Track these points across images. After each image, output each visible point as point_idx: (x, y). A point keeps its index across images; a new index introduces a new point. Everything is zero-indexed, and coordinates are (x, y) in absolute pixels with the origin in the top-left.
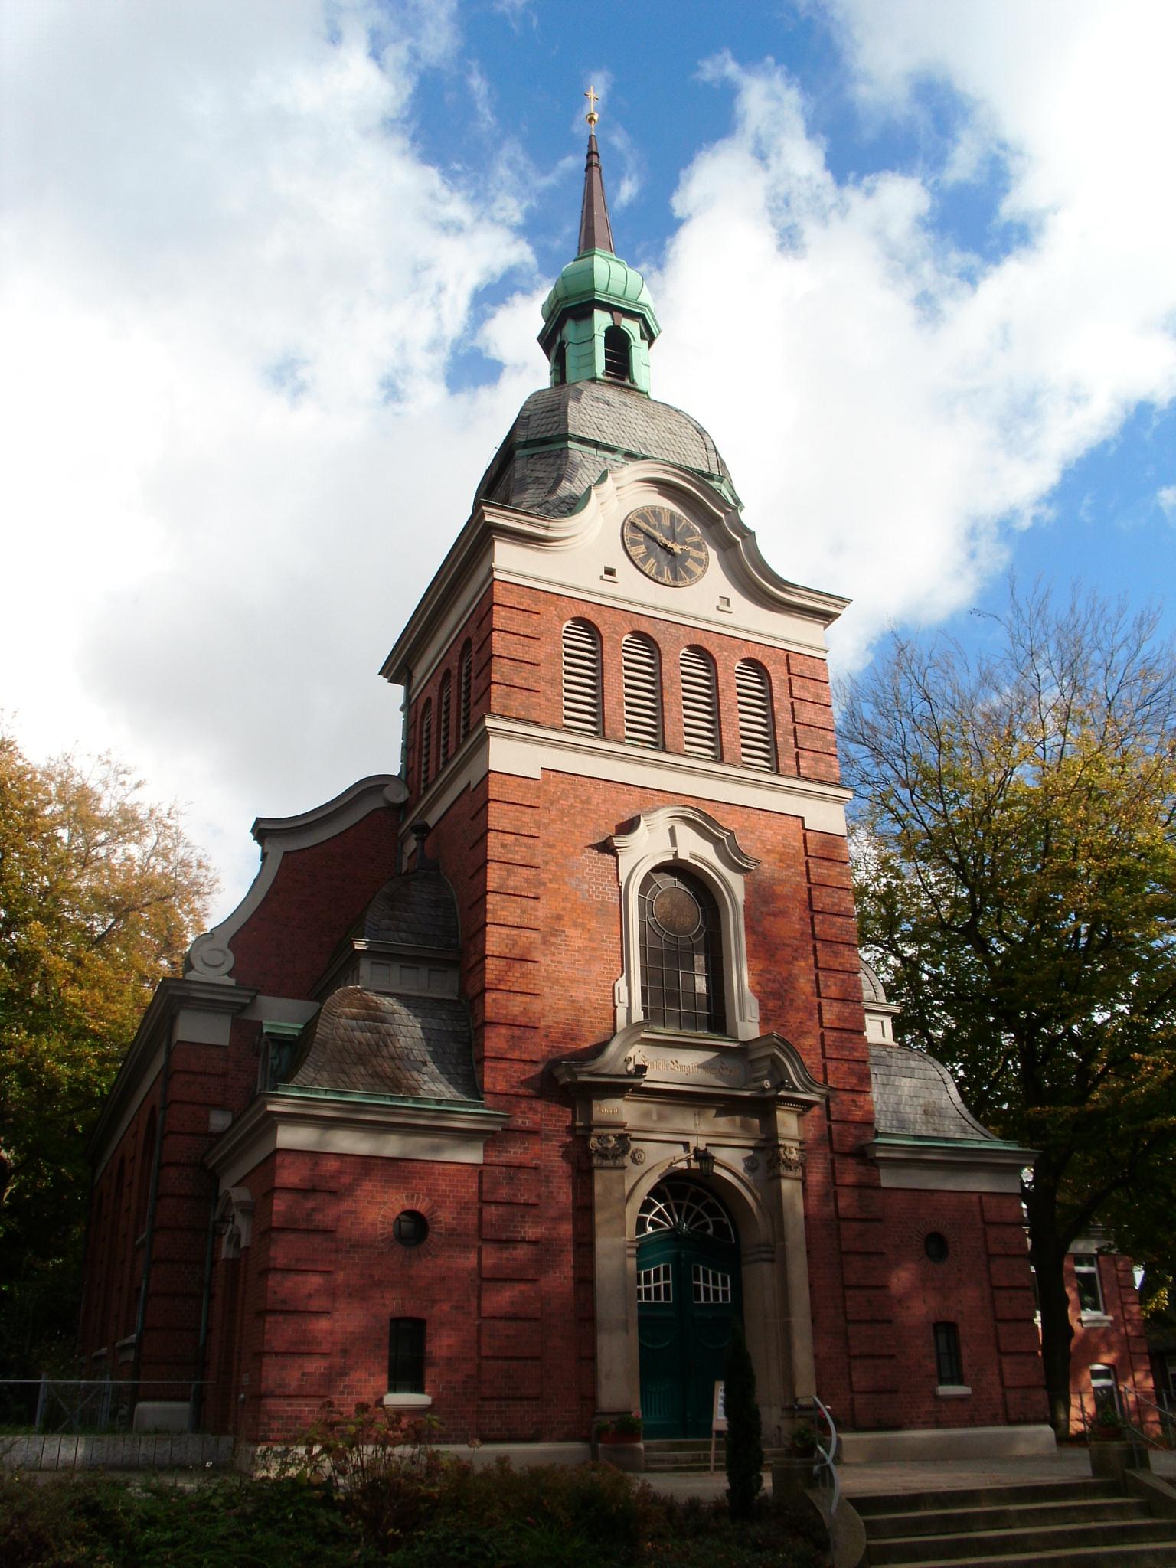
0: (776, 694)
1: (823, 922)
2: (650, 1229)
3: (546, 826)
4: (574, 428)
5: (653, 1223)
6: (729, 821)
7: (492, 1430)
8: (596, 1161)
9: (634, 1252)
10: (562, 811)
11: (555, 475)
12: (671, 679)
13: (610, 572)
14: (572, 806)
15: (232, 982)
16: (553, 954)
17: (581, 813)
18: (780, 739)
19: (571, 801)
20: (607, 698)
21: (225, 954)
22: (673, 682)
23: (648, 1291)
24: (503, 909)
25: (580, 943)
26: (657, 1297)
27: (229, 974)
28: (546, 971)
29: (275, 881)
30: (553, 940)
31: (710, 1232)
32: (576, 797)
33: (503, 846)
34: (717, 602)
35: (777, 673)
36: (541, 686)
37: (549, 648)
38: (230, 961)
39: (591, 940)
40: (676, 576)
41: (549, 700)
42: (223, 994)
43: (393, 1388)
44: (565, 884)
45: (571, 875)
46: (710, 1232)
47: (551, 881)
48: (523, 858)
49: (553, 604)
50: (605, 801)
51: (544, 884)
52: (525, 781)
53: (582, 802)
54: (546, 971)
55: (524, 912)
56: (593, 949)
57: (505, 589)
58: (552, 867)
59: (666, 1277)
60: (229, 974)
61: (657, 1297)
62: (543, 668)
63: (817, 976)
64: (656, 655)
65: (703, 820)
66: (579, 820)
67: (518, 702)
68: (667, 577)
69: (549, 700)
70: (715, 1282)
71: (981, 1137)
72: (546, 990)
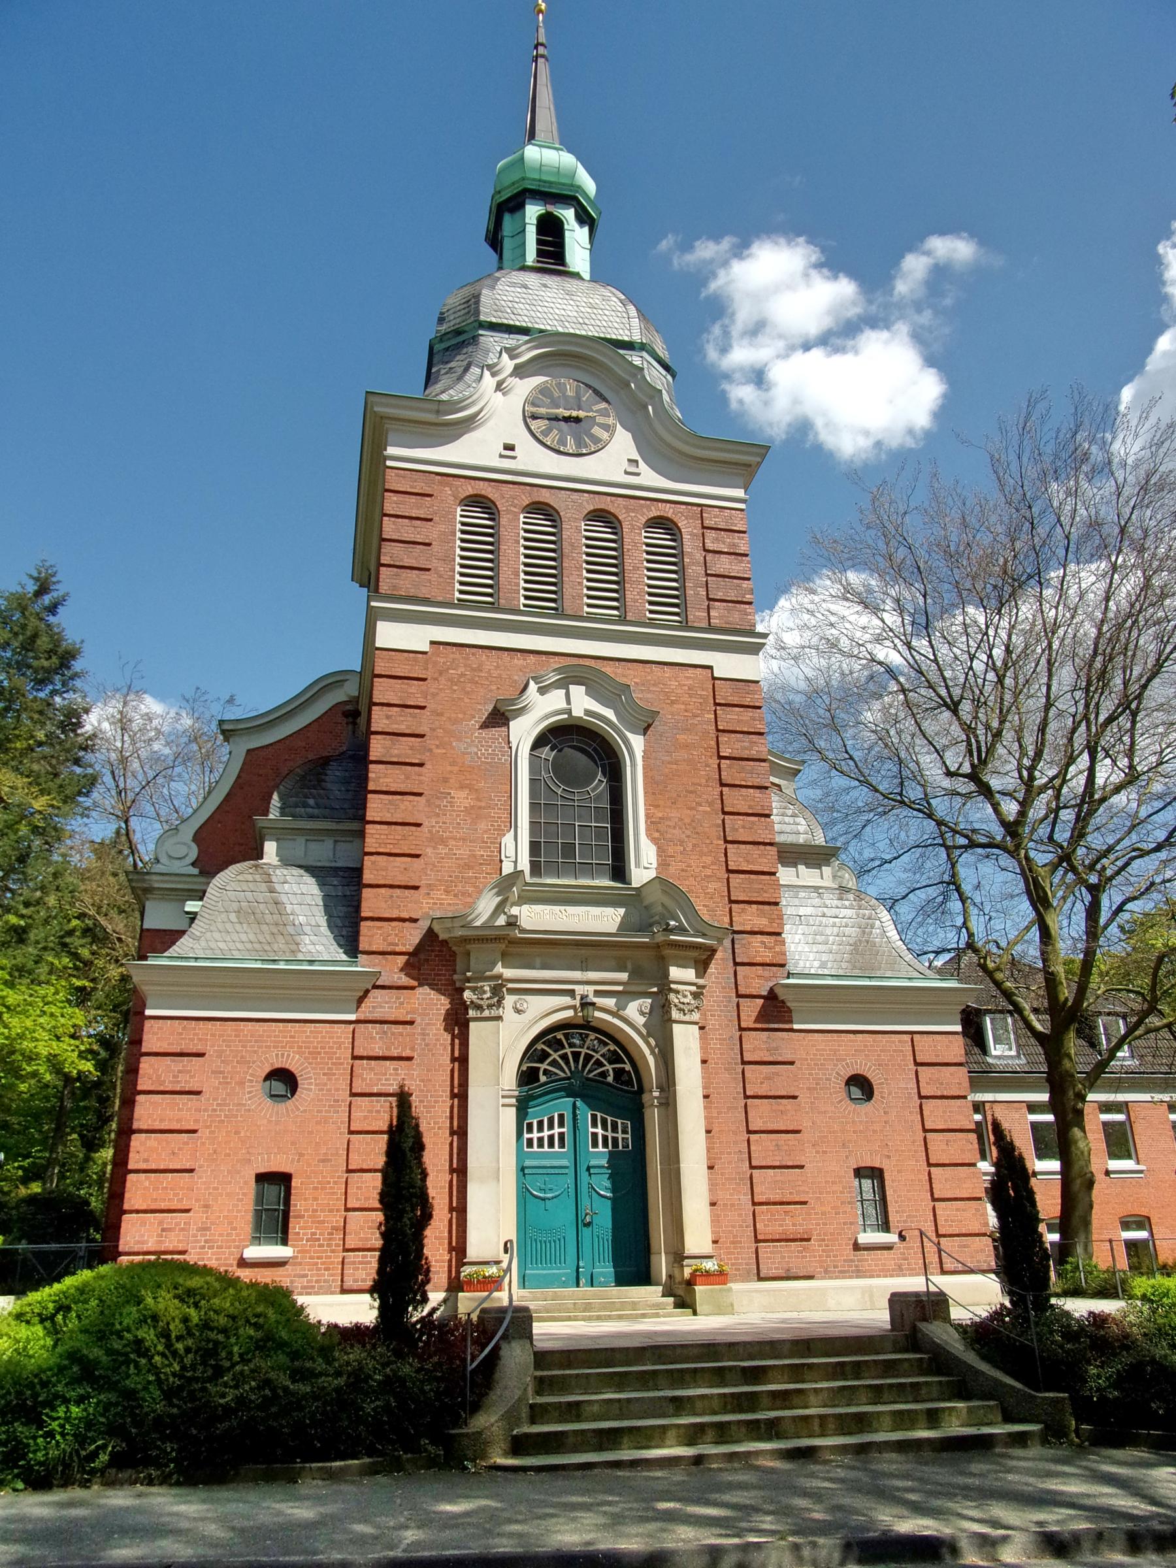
0: (687, 549)
1: (730, 767)
2: (543, 1079)
3: (434, 695)
4: (487, 314)
5: (546, 1072)
6: (629, 676)
7: (356, 1281)
8: (472, 1013)
9: (514, 1101)
10: (450, 680)
11: (465, 363)
12: (572, 545)
13: (510, 447)
14: (462, 675)
15: (196, 871)
16: (438, 815)
17: (472, 681)
18: (690, 592)
19: (461, 670)
20: (503, 568)
21: (189, 847)
22: (636, 568)
23: (540, 1140)
24: (386, 776)
25: (466, 803)
26: (551, 1145)
27: (193, 864)
28: (430, 832)
29: (239, 777)
30: (438, 802)
31: (610, 1079)
32: (465, 666)
33: (388, 717)
34: (626, 465)
35: (688, 528)
36: (434, 564)
37: (442, 527)
38: (194, 852)
39: (478, 799)
40: (579, 443)
41: (441, 576)
42: (185, 882)
43: (257, 1240)
44: (453, 748)
45: (459, 740)
46: (610, 1079)
47: (438, 747)
48: (408, 727)
49: (448, 485)
50: (497, 667)
51: (430, 750)
52: (411, 655)
53: (473, 670)
54: (430, 832)
55: (407, 778)
56: (480, 808)
57: (397, 475)
58: (440, 732)
59: (561, 1125)
60: (193, 864)
61: (551, 1145)
62: (436, 547)
63: (723, 821)
64: (558, 523)
65: (577, 672)
66: (468, 687)
67: (407, 582)
68: (571, 447)
69: (441, 576)
70: (615, 1129)
71: (916, 974)
72: (429, 850)
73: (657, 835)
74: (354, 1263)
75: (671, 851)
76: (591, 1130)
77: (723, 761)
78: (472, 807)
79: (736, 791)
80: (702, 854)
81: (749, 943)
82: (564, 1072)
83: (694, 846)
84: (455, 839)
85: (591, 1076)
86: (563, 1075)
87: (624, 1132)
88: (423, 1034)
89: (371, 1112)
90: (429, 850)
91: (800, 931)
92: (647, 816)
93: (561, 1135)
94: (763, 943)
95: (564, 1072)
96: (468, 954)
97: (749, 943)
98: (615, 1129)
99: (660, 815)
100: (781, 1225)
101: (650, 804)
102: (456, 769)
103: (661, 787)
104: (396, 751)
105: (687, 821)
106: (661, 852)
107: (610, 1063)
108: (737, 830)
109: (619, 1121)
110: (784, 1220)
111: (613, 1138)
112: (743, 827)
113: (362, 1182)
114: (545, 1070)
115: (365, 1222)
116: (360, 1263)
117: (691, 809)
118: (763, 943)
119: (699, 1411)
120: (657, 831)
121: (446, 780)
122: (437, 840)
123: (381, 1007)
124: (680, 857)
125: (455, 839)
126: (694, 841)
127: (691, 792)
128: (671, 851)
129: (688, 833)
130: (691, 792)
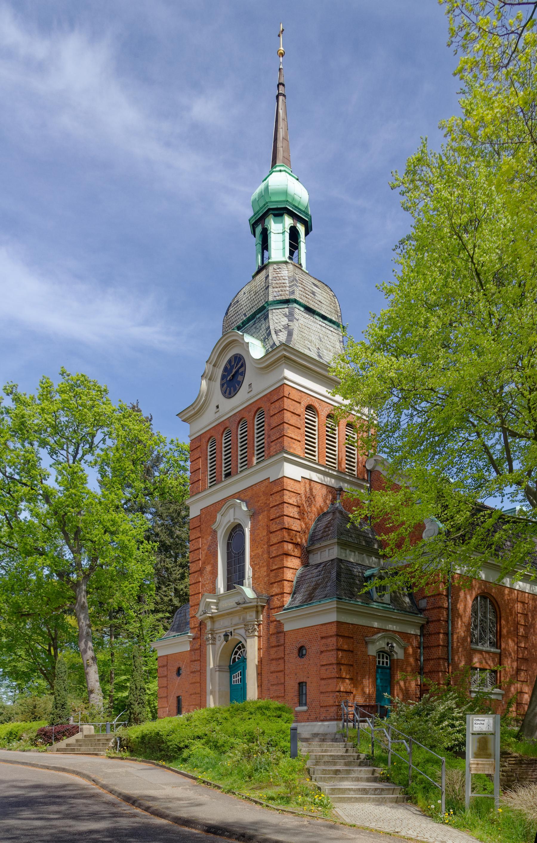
106: (253, 569)
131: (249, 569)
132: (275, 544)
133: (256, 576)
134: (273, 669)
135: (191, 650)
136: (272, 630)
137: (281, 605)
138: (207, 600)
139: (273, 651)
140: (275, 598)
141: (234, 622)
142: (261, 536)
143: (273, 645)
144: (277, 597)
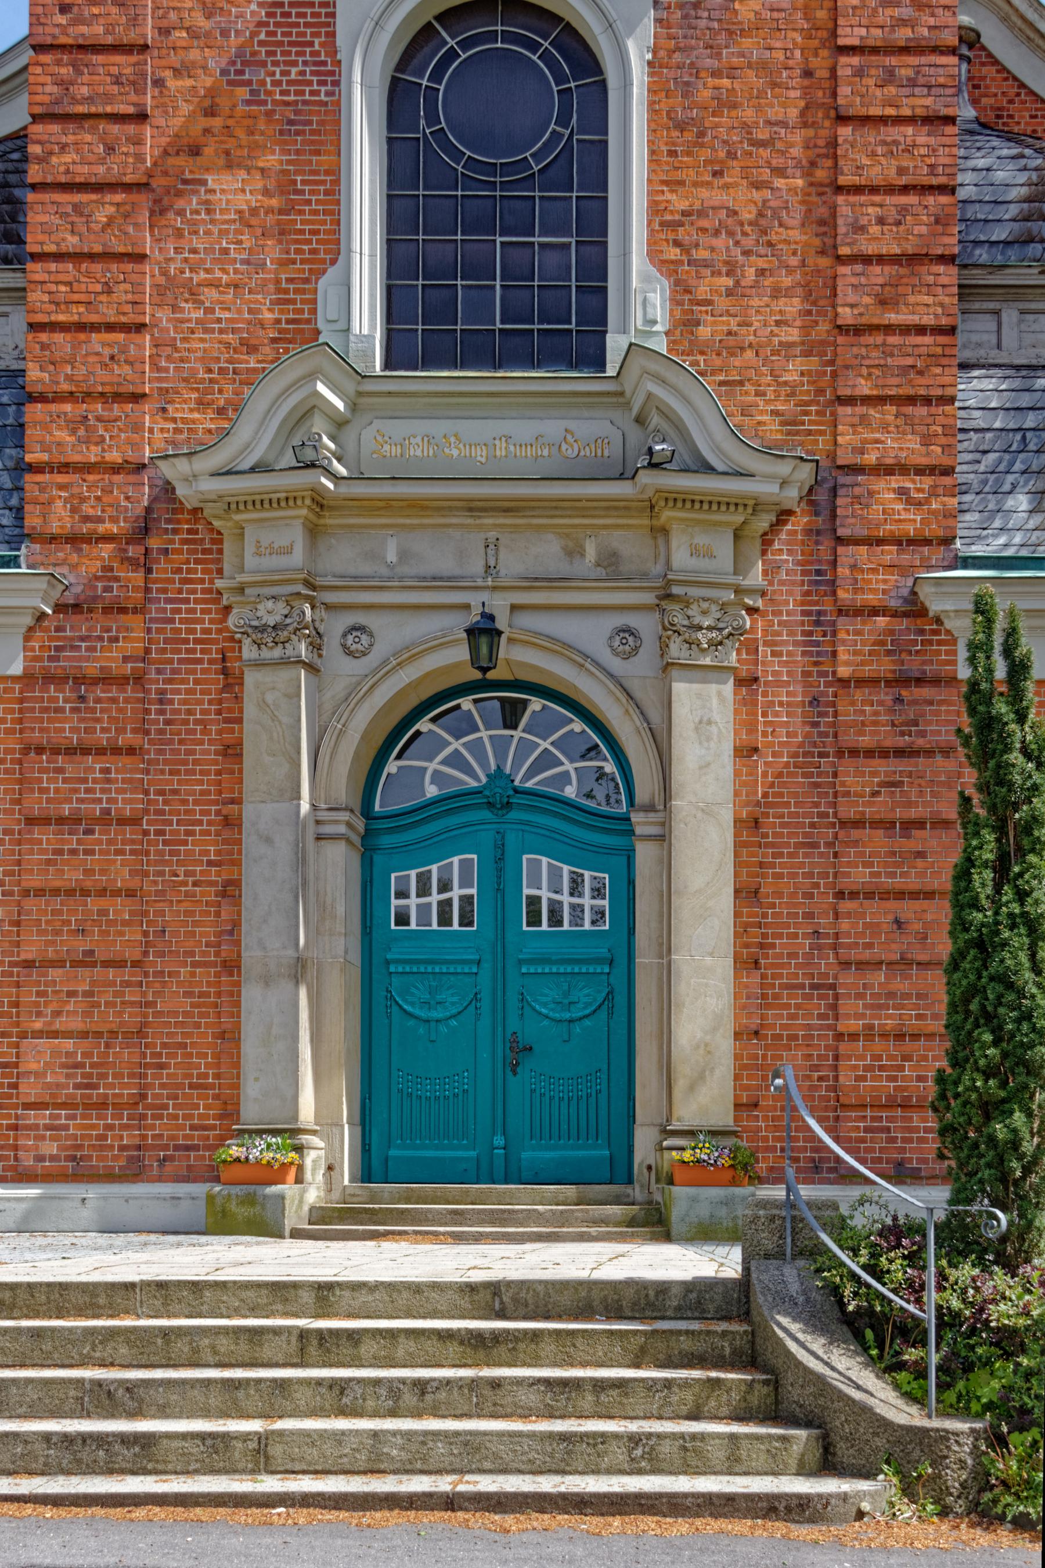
1: (859, 73)
28: (164, 273)
55: (110, 149)
59: (465, 883)
73: (674, 253)
74: (36, 1127)
75: (702, 291)
76: (527, 891)
77: (843, 60)
78: (254, 211)
79: (870, 136)
80: (776, 293)
81: (871, 493)
82: (476, 778)
83: (761, 272)
84: (215, 284)
85: (529, 784)
86: (475, 784)
87: (598, 892)
88: (161, 702)
89: (59, 852)
90: (163, 315)
91: (1018, 466)
92: (655, 209)
93: (466, 900)
94: (902, 492)
95: (476, 778)
96: (240, 535)
97: (871, 493)
98: (576, 889)
99: (683, 205)
100: (894, 1079)
101: (665, 178)
102: (217, 122)
103: (689, 136)
104: (85, 90)
105: (748, 214)
106: (682, 291)
107: (572, 761)
108: (862, 229)
109: (587, 874)
110: (901, 1068)
111: (573, 907)
112: (881, 221)
113: (46, 984)
114: (436, 772)
115: (55, 1054)
116: (47, 1127)
117: (757, 185)
118: (902, 492)
119: (278, 1463)
120: (677, 243)
121: (195, 151)
122: (169, 290)
123: (74, 648)
124: (722, 303)
125: (215, 284)
126: (762, 263)
127: (762, 144)
128: (702, 291)
129: (748, 242)
130: (762, 144)
131: (646, 279)
132: (874, 190)
133: (704, 332)
134: (860, 876)
135: (27, 678)
136: (855, 649)
137: (935, 529)
138: (321, 388)
139: (859, 780)
140: (886, 488)
141: (512, 563)
142: (748, 114)
143: (865, 741)
144: (896, 481)
